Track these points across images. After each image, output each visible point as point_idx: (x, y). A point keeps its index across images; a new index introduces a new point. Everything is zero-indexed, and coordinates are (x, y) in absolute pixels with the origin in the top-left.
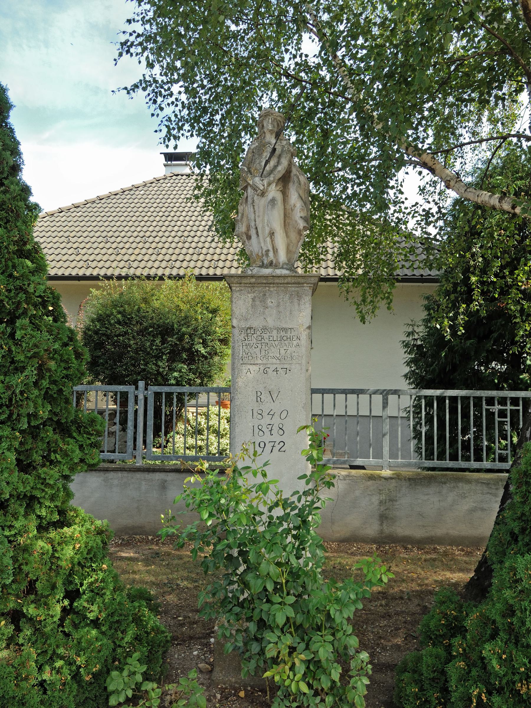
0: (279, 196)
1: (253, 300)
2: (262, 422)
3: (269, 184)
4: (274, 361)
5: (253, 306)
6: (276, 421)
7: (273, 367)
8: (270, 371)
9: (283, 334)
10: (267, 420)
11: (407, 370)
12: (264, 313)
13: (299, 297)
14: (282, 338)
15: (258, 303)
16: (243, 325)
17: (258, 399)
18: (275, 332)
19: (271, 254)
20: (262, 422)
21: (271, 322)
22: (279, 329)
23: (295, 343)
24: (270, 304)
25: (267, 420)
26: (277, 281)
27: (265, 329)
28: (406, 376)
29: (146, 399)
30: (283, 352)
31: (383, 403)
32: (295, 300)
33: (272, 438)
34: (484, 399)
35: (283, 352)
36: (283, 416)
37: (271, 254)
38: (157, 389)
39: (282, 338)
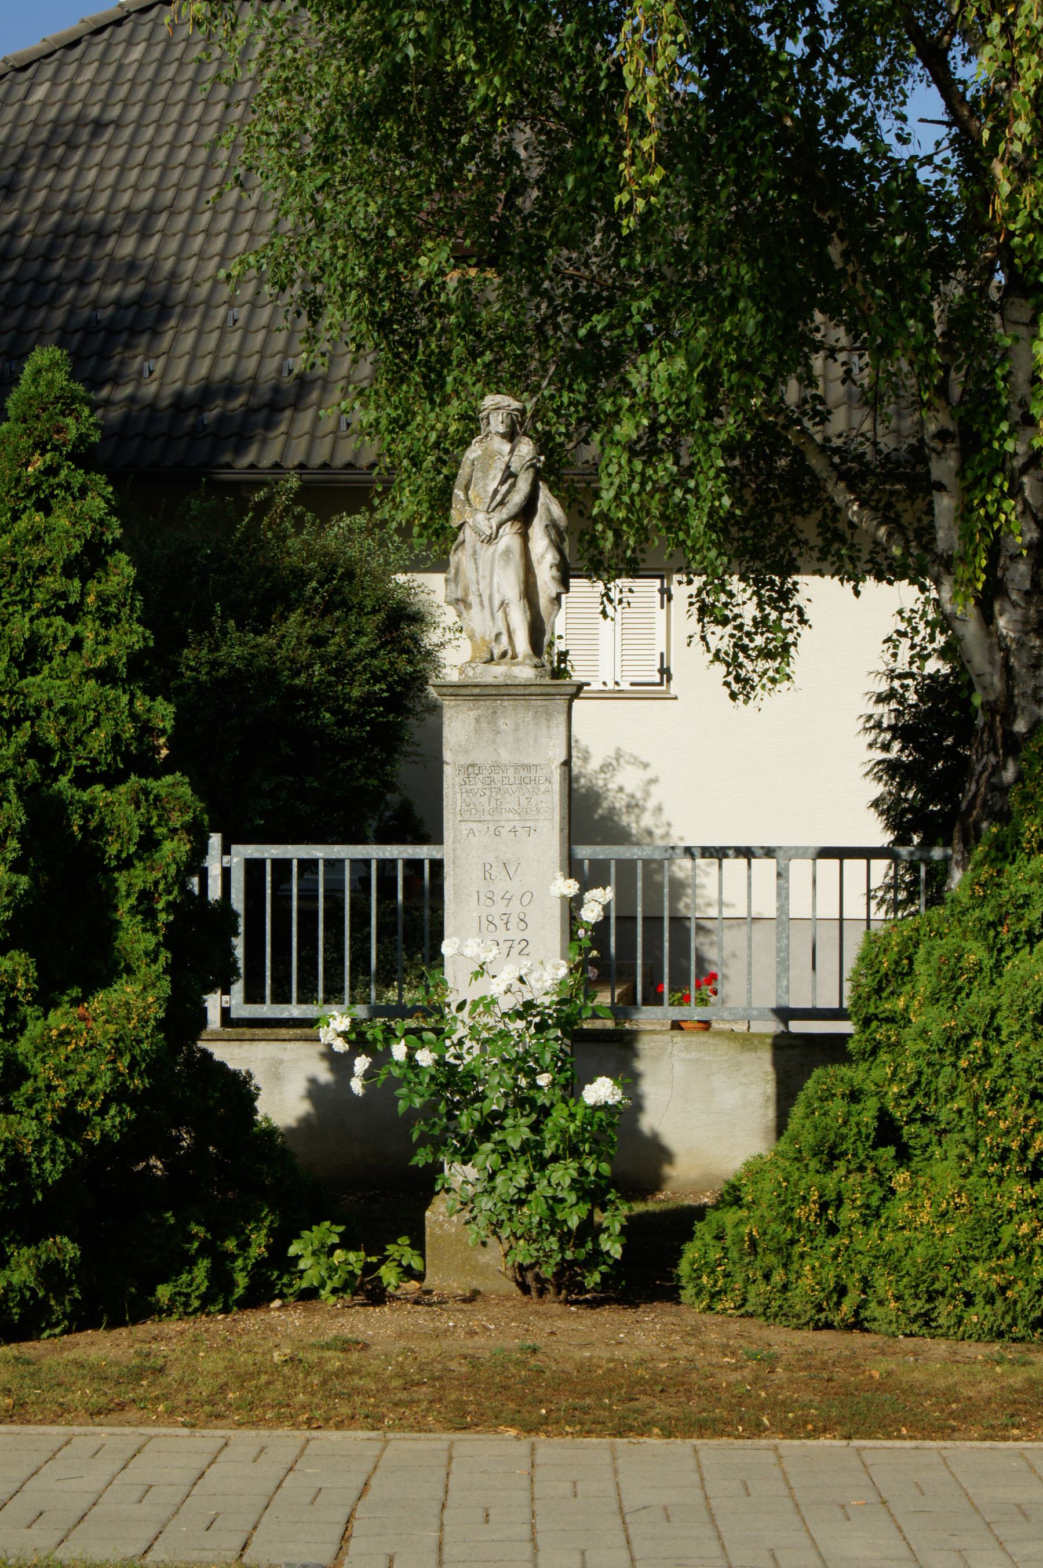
0: (516, 543)
1: (478, 720)
2: (493, 910)
3: (500, 526)
4: (511, 816)
5: (478, 731)
6: (515, 908)
7: (509, 826)
8: (504, 832)
9: (523, 773)
10: (500, 907)
11: (878, 789)
12: (494, 741)
13: (549, 716)
14: (522, 780)
15: (484, 725)
16: (462, 760)
17: (487, 876)
18: (511, 771)
19: (504, 639)
20: (493, 910)
21: (505, 756)
22: (518, 767)
23: (542, 788)
24: (503, 727)
25: (500, 907)
26: (513, 691)
27: (496, 766)
28: (876, 804)
29: (226, 872)
30: (523, 801)
31: (779, 894)
32: (543, 721)
33: (509, 935)
34: (347, 863)
35: (523, 801)
36: (525, 901)
37: (504, 639)
38: (253, 851)
39: (522, 780)
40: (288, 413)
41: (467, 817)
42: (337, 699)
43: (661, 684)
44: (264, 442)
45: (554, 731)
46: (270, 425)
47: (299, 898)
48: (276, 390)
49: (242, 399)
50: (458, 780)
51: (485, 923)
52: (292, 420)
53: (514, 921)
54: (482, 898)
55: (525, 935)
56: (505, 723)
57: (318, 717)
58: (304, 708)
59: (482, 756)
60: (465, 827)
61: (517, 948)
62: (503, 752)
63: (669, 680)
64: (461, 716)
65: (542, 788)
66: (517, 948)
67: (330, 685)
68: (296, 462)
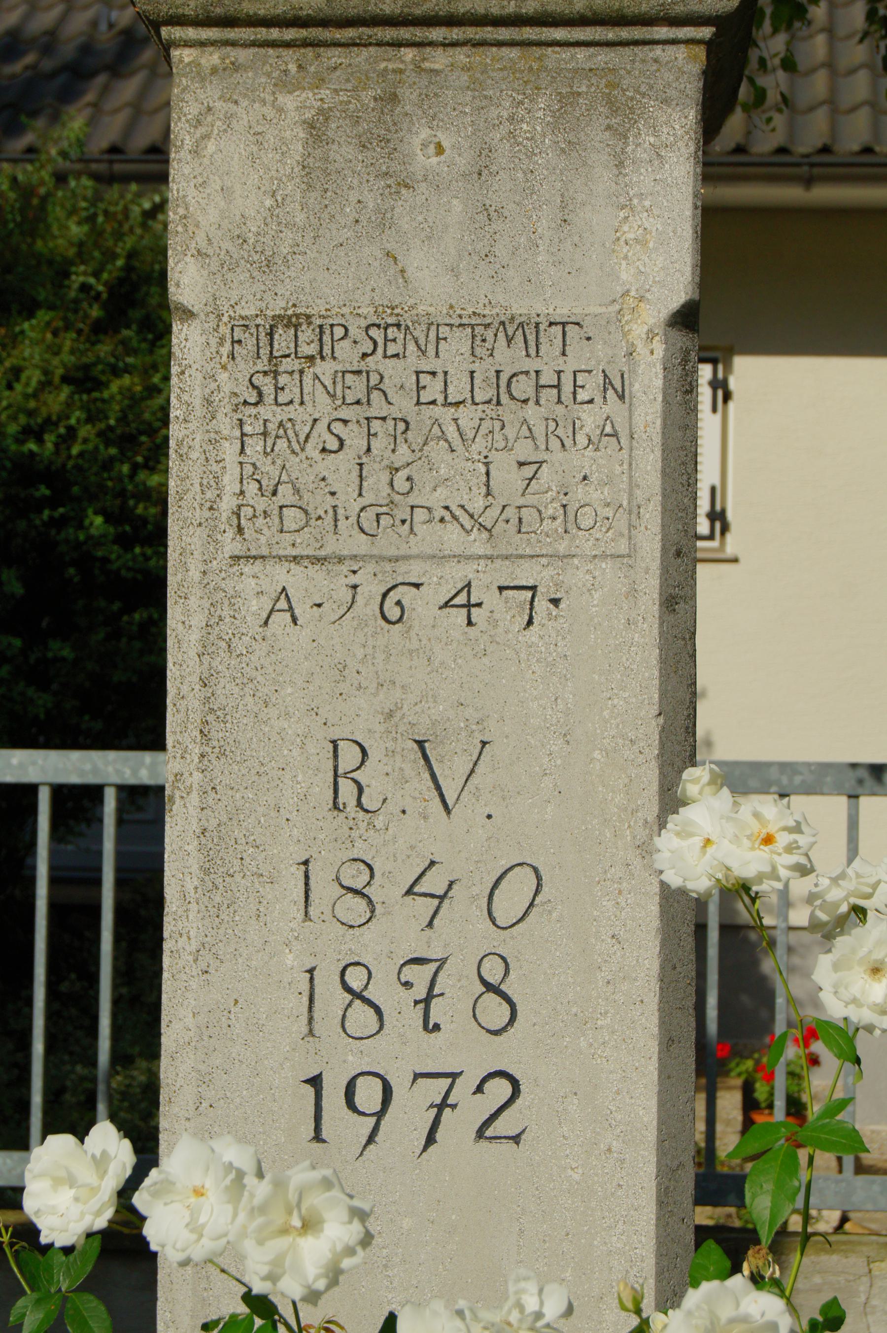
1: (316, 130)
4: (452, 537)
5: (315, 175)
6: (463, 935)
7: (443, 581)
8: (422, 606)
9: (509, 357)
10: (400, 929)
12: (384, 221)
13: (622, 115)
14: (503, 383)
15: (344, 151)
16: (250, 298)
17: (345, 789)
18: (457, 344)
21: (433, 284)
22: (478, 329)
23: (589, 420)
25: (400, 929)
27: (389, 328)
32: (596, 135)
33: (438, 1053)
36: (509, 905)
39: (503, 383)
40: (101, 79)
41: (263, 536)
42: (122, 494)
43: (711, 537)
44: (55, 118)
45: (642, 178)
46: (68, 95)
47: (53, 881)
48: (86, 49)
49: (29, 59)
50: (232, 382)
51: (331, 997)
52: (106, 90)
53: (457, 989)
54: (324, 890)
55: (505, 1053)
56: (435, 144)
57: (80, 526)
58: (53, 503)
59: (333, 283)
60: (254, 587)
61: (472, 1108)
62: (420, 262)
63: (725, 529)
64: (246, 114)
65: (589, 420)
66: (472, 1108)
67: (108, 465)
68: (105, 144)
